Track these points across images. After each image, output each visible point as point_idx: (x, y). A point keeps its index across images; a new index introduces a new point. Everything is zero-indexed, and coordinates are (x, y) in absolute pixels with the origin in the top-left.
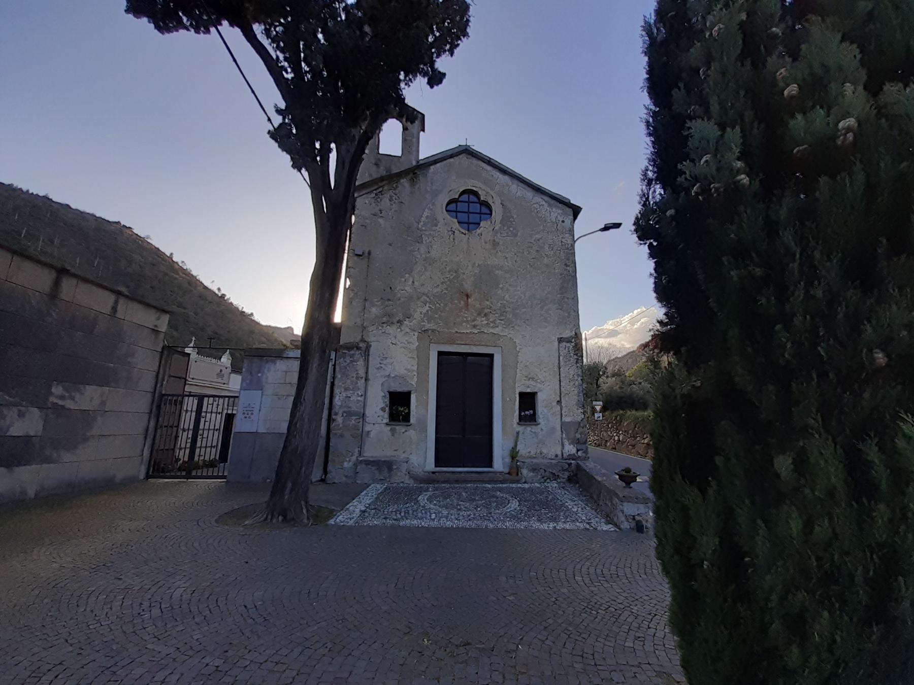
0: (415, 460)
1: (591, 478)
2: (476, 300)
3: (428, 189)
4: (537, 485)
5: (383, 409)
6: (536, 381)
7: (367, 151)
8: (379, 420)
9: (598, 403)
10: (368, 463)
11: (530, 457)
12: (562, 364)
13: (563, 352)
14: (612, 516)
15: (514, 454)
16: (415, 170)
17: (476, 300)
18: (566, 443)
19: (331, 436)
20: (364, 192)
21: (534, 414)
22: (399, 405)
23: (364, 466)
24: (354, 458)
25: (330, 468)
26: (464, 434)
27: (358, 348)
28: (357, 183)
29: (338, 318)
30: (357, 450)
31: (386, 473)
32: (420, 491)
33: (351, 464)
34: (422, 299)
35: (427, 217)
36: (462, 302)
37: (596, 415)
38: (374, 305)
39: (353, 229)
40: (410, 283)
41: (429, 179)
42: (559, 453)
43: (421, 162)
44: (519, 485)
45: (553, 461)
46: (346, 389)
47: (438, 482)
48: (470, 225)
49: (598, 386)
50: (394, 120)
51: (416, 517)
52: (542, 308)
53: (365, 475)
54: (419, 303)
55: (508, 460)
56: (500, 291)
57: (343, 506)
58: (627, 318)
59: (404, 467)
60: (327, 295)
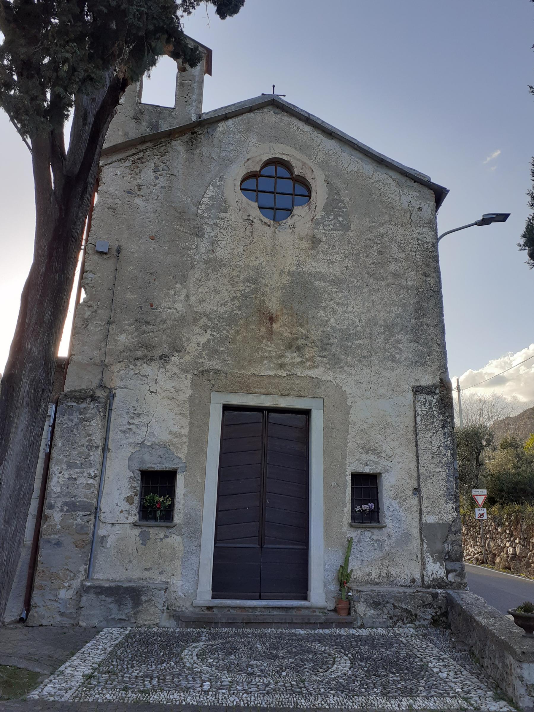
0: (180, 585)
1: (468, 619)
2: (284, 325)
3: (215, 156)
4: (381, 631)
6: (378, 455)
7: (122, 101)
8: (122, 518)
9: (480, 491)
10: (100, 590)
11: (371, 583)
12: (420, 428)
13: (422, 410)
14: (504, 685)
15: (343, 578)
16: (197, 129)
17: (284, 325)
18: (429, 559)
19: (41, 544)
20: (115, 158)
22: (156, 491)
23: (92, 596)
24: (76, 583)
25: (36, 599)
26: (261, 547)
27: (94, 399)
28: (105, 146)
29: (63, 351)
30: (82, 569)
31: (129, 609)
32: (187, 640)
33: (71, 592)
35: (211, 198)
36: (263, 329)
37: (478, 511)
38: (124, 331)
39: (95, 215)
40: (183, 297)
41: (215, 142)
43: (204, 117)
44: (353, 631)
45: (408, 590)
46: (69, 466)
47: (216, 624)
48: (277, 212)
49: (479, 464)
50: (166, 56)
51: (178, 688)
52: (387, 340)
53: (93, 611)
55: (333, 587)
56: (321, 313)
57: (55, 665)
58: (519, 357)
59: (160, 599)
60: (48, 315)
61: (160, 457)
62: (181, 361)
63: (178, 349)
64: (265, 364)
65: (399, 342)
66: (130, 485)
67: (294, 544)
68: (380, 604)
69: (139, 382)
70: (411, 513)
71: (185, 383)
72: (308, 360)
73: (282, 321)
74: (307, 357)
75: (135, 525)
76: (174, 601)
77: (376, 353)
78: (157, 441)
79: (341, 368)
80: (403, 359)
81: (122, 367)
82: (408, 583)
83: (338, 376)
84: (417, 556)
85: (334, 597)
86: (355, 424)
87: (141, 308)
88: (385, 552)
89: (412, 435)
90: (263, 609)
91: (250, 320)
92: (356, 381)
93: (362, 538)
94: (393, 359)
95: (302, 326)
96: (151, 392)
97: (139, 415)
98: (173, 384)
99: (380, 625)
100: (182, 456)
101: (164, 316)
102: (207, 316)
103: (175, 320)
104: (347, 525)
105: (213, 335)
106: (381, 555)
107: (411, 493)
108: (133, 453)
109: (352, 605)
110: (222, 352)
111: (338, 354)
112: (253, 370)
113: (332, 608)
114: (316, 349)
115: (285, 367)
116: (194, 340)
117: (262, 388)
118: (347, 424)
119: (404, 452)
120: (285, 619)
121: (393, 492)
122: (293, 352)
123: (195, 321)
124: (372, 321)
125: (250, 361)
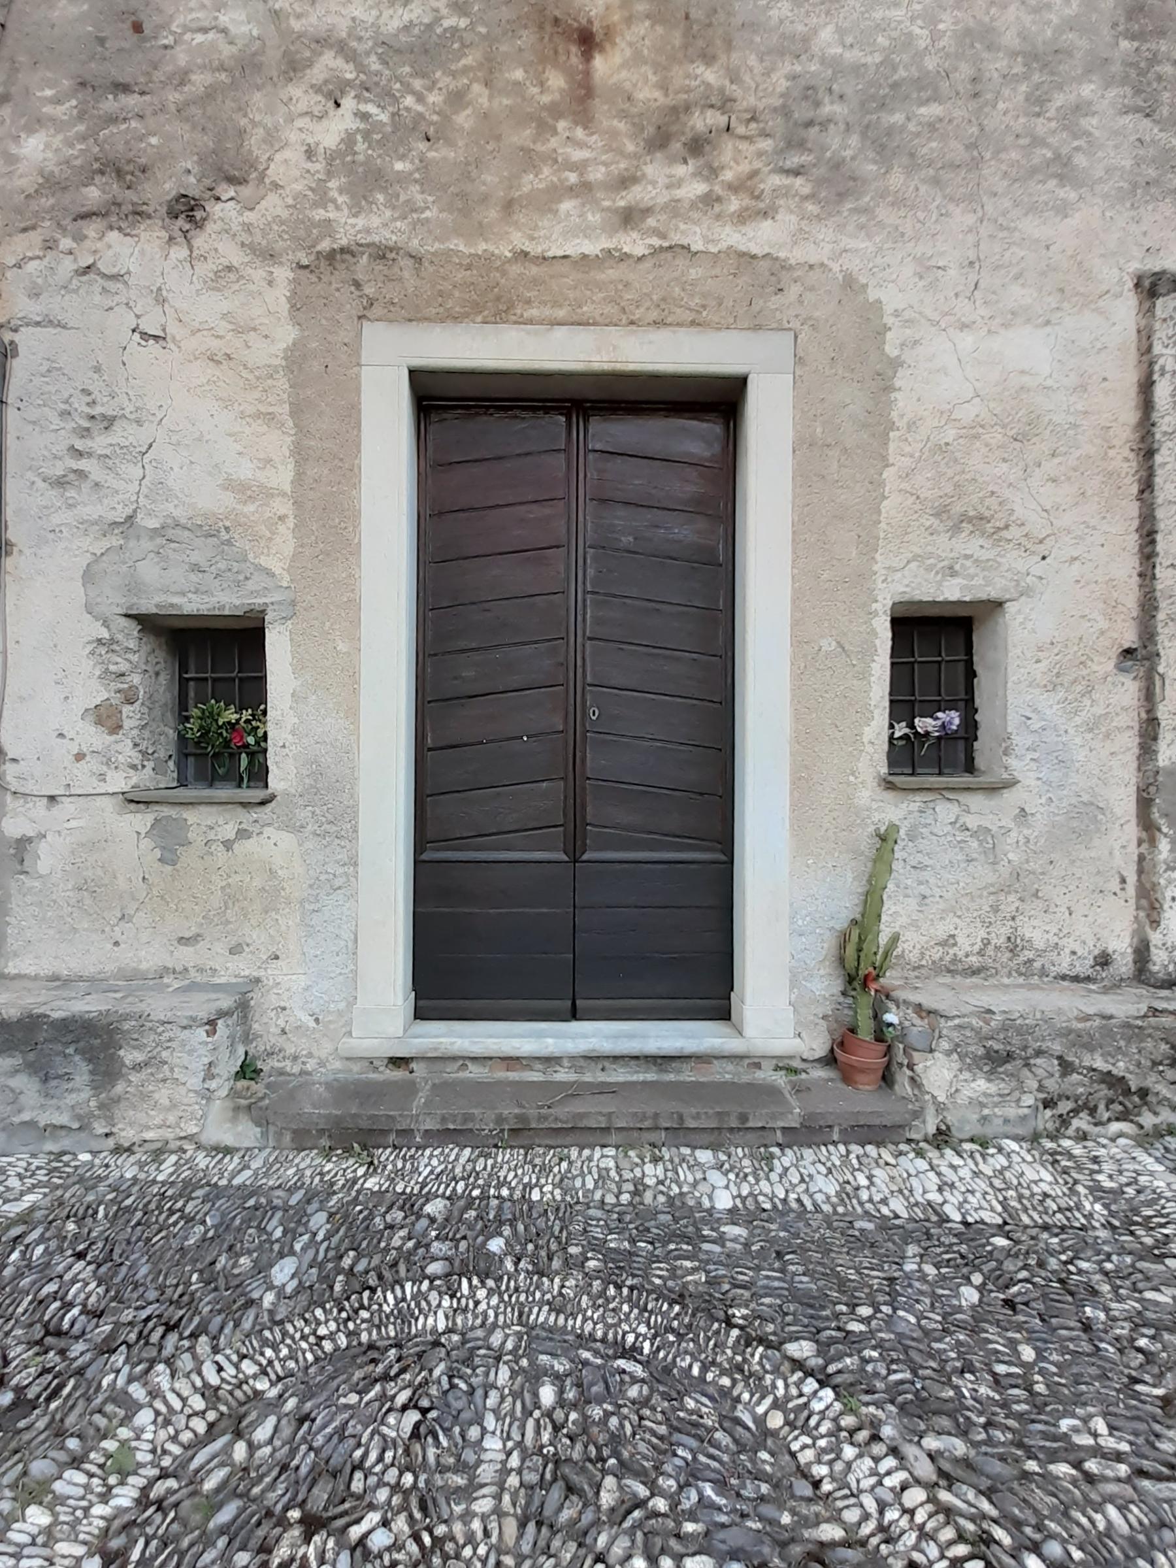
2: (637, 59)
5: (106, 718)
8: (83, 777)
11: (953, 969)
15: (860, 968)
17: (637, 59)
21: (970, 728)
22: (208, 682)
31: (79, 1092)
34: (317, 73)
38: (37, 123)
42: (1121, 945)
52: (1037, 102)
54: (300, 95)
55: (825, 985)
61: (196, 568)
62: (249, 217)
63: (233, 171)
64: (568, 215)
65: (1081, 108)
66: (102, 668)
67: (691, 848)
68: (1009, 1057)
69: (97, 299)
70: (1107, 736)
71: (271, 294)
72: (734, 188)
73: (630, 44)
74: (728, 175)
75: (134, 801)
76: (281, 1041)
77: (997, 152)
78: (180, 514)
79: (865, 210)
80: (1099, 173)
81: (30, 247)
82: (1083, 968)
83: (852, 244)
84: (1123, 881)
85: (824, 1017)
86: (911, 426)
87: (101, 41)
88: (1004, 870)
89: (1127, 460)
90: (582, 1063)
91: (504, 48)
92: (919, 260)
93: (926, 825)
94: (1062, 169)
95: (708, 59)
96: (145, 336)
97: (109, 422)
98: (225, 306)
99: (1008, 1129)
100: (277, 567)
101: (182, 58)
102: (342, 49)
103: (222, 68)
104: (872, 783)
105: (365, 116)
106: (991, 878)
107: (1110, 666)
108: (97, 558)
109: (900, 1057)
110: (403, 179)
111: (853, 158)
112: (519, 240)
113: (821, 1051)
114: (766, 144)
115: (643, 220)
116: (293, 137)
117: (556, 304)
118: (879, 426)
119: (1093, 522)
120: (656, 1116)
121: (1042, 666)
122: (672, 160)
123: (293, 67)
124: (980, 37)
125: (509, 206)
